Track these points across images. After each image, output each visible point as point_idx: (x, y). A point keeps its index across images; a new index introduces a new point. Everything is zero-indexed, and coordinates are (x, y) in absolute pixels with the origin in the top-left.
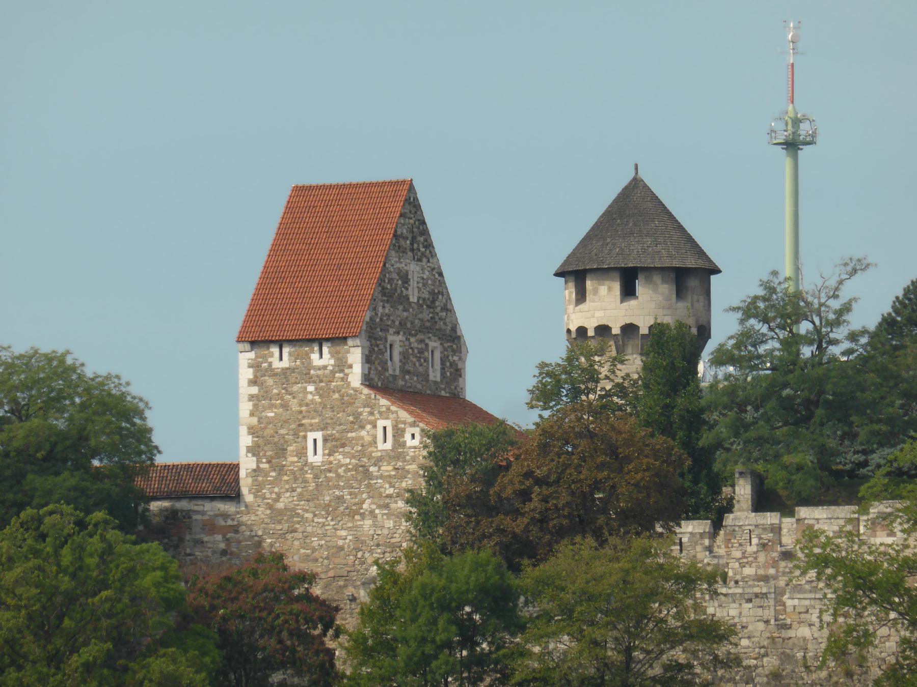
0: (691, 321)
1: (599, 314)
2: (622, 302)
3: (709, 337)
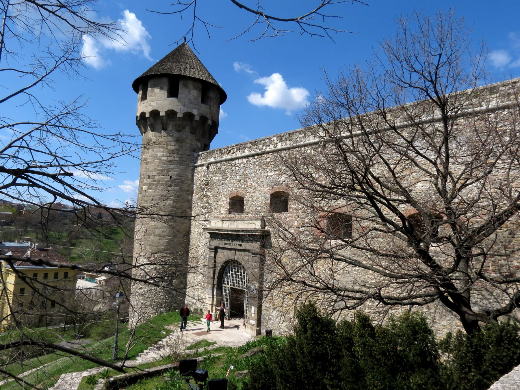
0: (209, 116)
1: (153, 103)
2: (168, 97)
3: (217, 133)
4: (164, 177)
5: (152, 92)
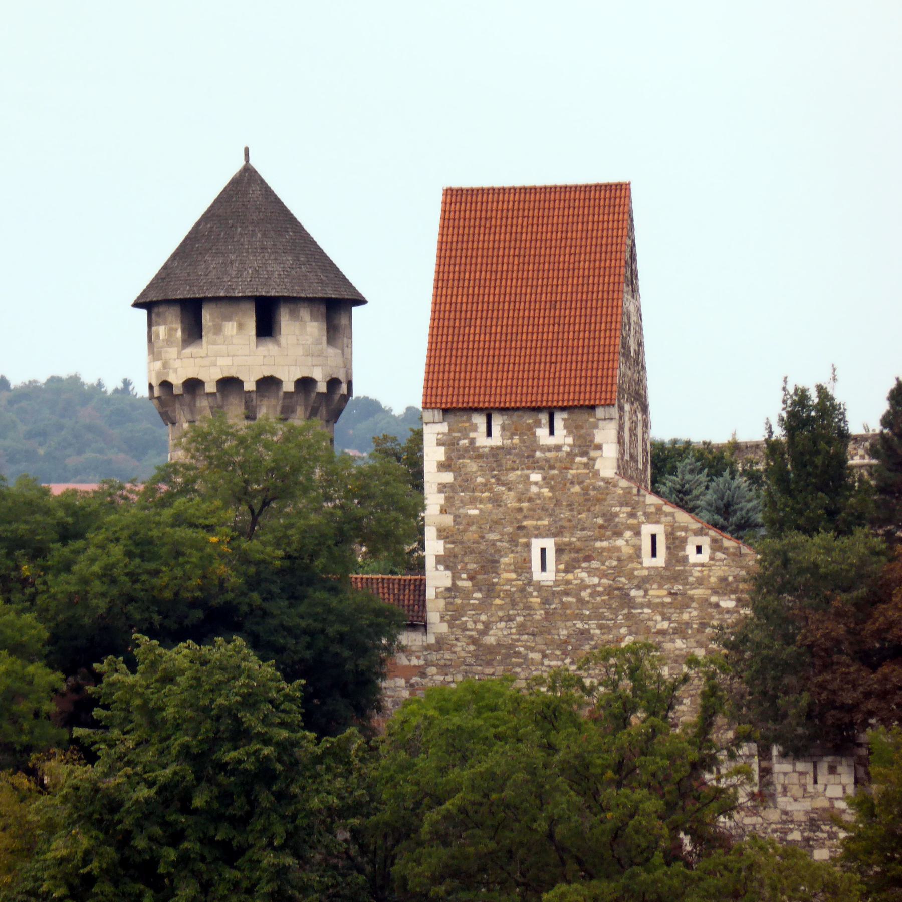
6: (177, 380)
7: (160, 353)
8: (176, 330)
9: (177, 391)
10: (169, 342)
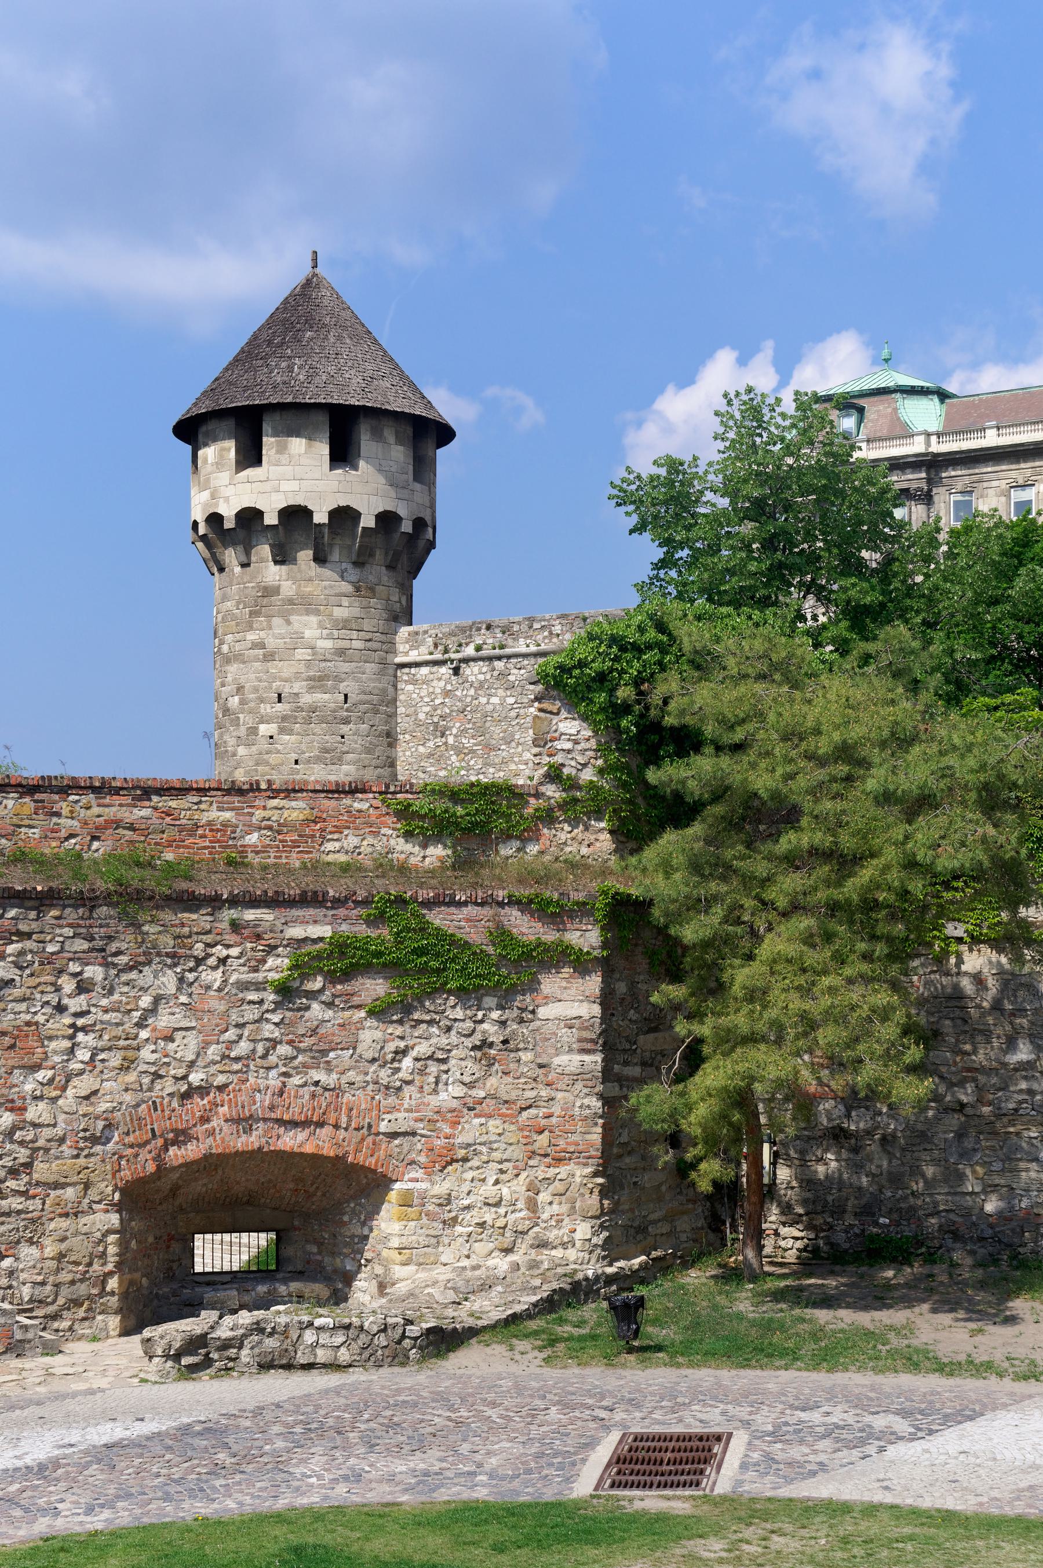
4: (327, 696)
5: (278, 452)
6: (229, 511)
7: (208, 480)
8: (229, 449)
9: (229, 524)
10: (219, 465)
